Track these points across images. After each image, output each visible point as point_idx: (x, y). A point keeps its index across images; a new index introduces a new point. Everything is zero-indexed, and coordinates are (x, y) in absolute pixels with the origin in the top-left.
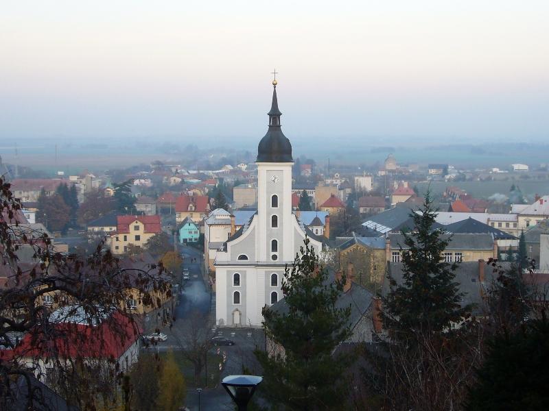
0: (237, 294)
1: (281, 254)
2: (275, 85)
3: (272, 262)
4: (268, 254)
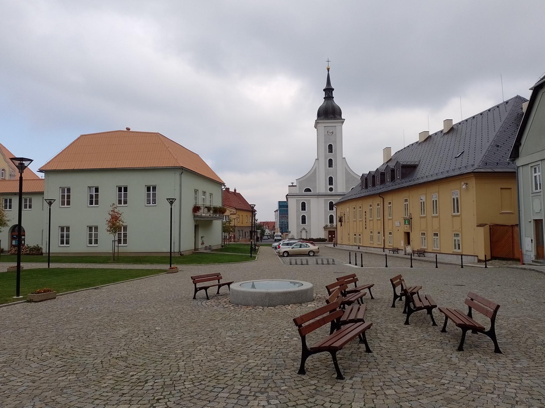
1: (336, 187)
2: (328, 69)
4: (326, 187)
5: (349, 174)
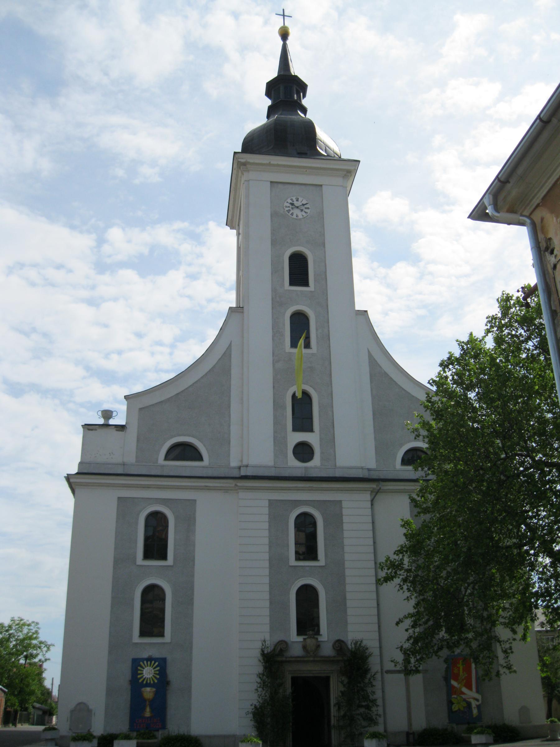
0: (153, 596)
1: (329, 441)
2: (284, 35)
3: (294, 465)
4: (279, 441)
5: (383, 374)
